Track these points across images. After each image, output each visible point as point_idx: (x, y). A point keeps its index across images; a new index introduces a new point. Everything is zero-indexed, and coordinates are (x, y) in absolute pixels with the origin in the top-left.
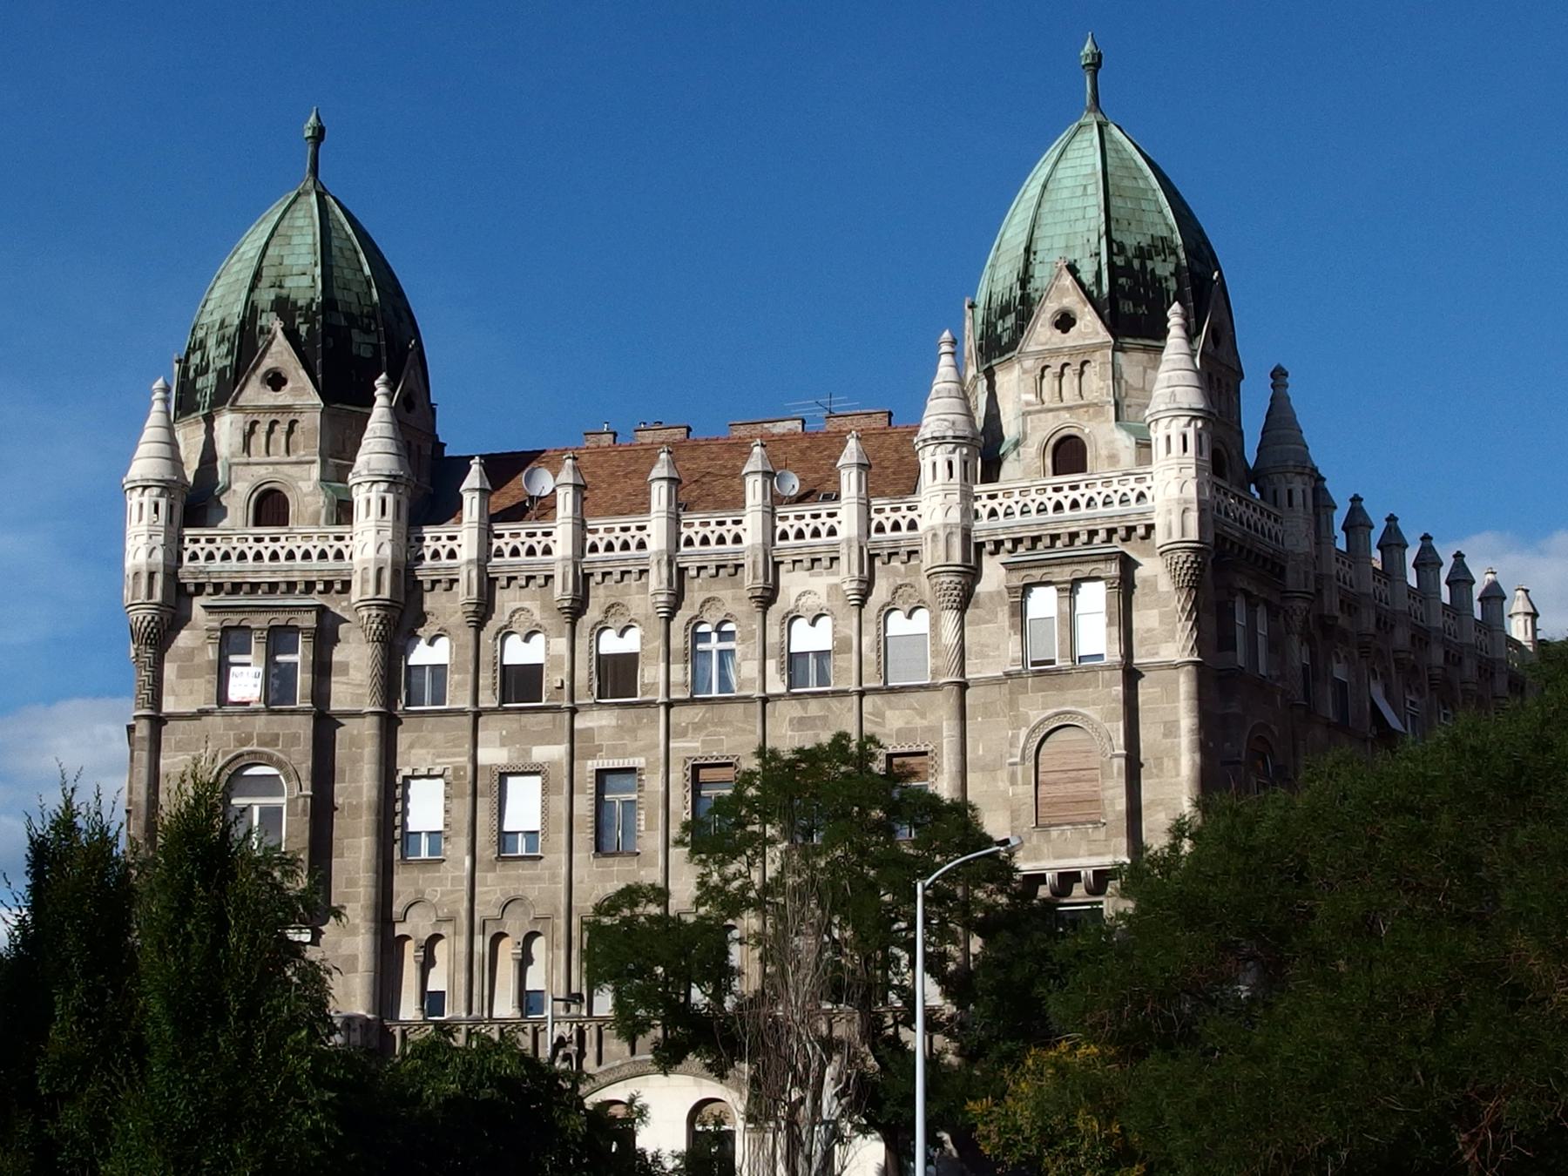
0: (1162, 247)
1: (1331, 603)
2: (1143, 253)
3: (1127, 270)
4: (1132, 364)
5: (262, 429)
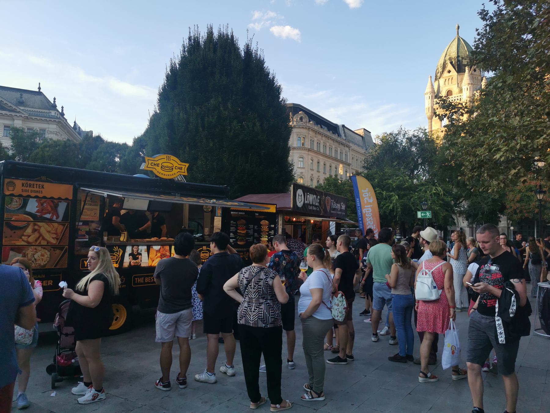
5: (447, 80)
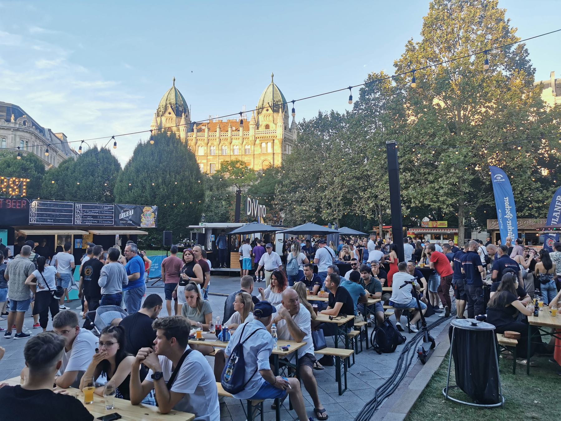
0: (280, 101)
2: (277, 102)
4: (275, 114)
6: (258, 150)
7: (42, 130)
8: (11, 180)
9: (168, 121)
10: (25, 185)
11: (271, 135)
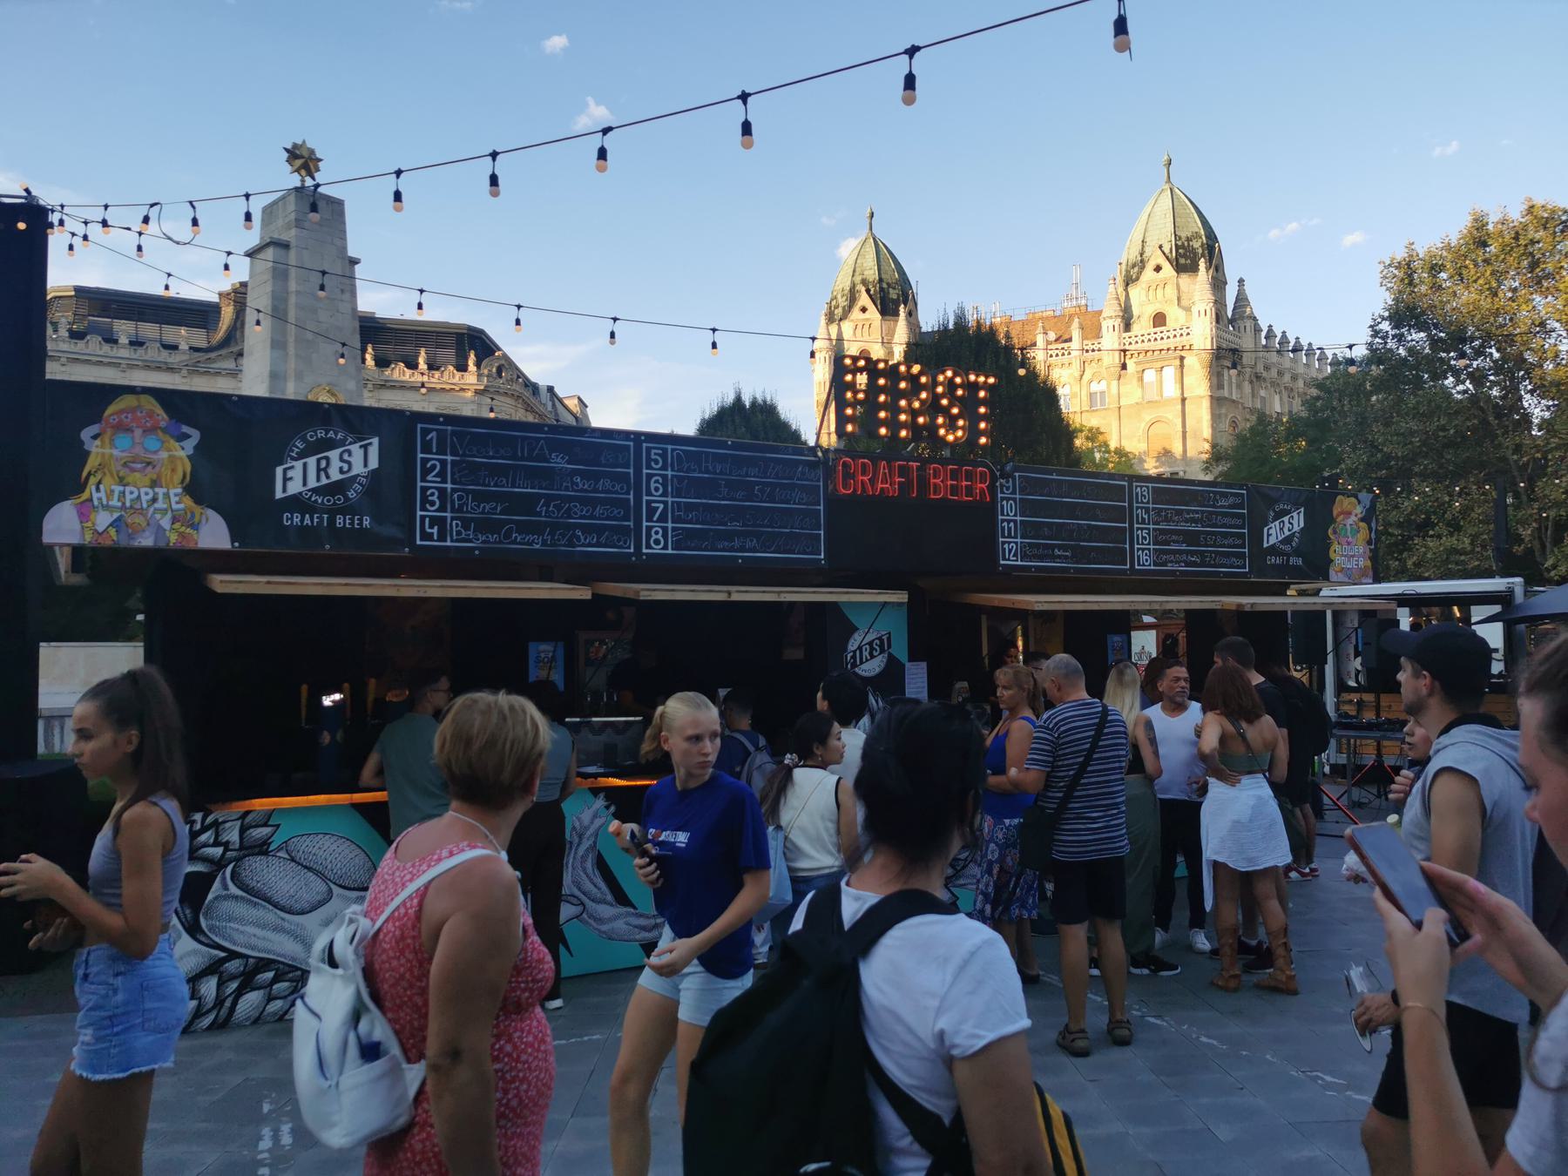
0: (1197, 236)
1: (1260, 368)
2: (1188, 240)
3: (1183, 247)
4: (1185, 279)
6: (1131, 393)
7: (534, 388)
8: (941, 378)
9: (859, 331)
10: (983, 402)
11: (1171, 343)
